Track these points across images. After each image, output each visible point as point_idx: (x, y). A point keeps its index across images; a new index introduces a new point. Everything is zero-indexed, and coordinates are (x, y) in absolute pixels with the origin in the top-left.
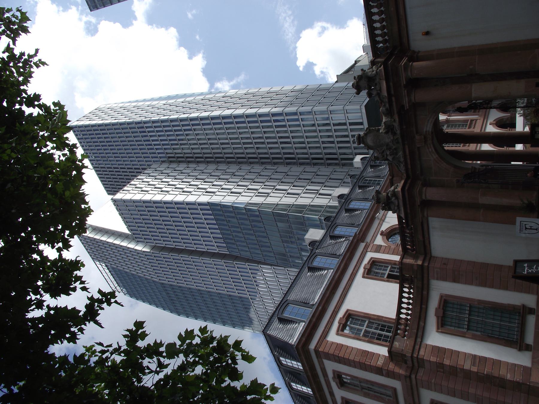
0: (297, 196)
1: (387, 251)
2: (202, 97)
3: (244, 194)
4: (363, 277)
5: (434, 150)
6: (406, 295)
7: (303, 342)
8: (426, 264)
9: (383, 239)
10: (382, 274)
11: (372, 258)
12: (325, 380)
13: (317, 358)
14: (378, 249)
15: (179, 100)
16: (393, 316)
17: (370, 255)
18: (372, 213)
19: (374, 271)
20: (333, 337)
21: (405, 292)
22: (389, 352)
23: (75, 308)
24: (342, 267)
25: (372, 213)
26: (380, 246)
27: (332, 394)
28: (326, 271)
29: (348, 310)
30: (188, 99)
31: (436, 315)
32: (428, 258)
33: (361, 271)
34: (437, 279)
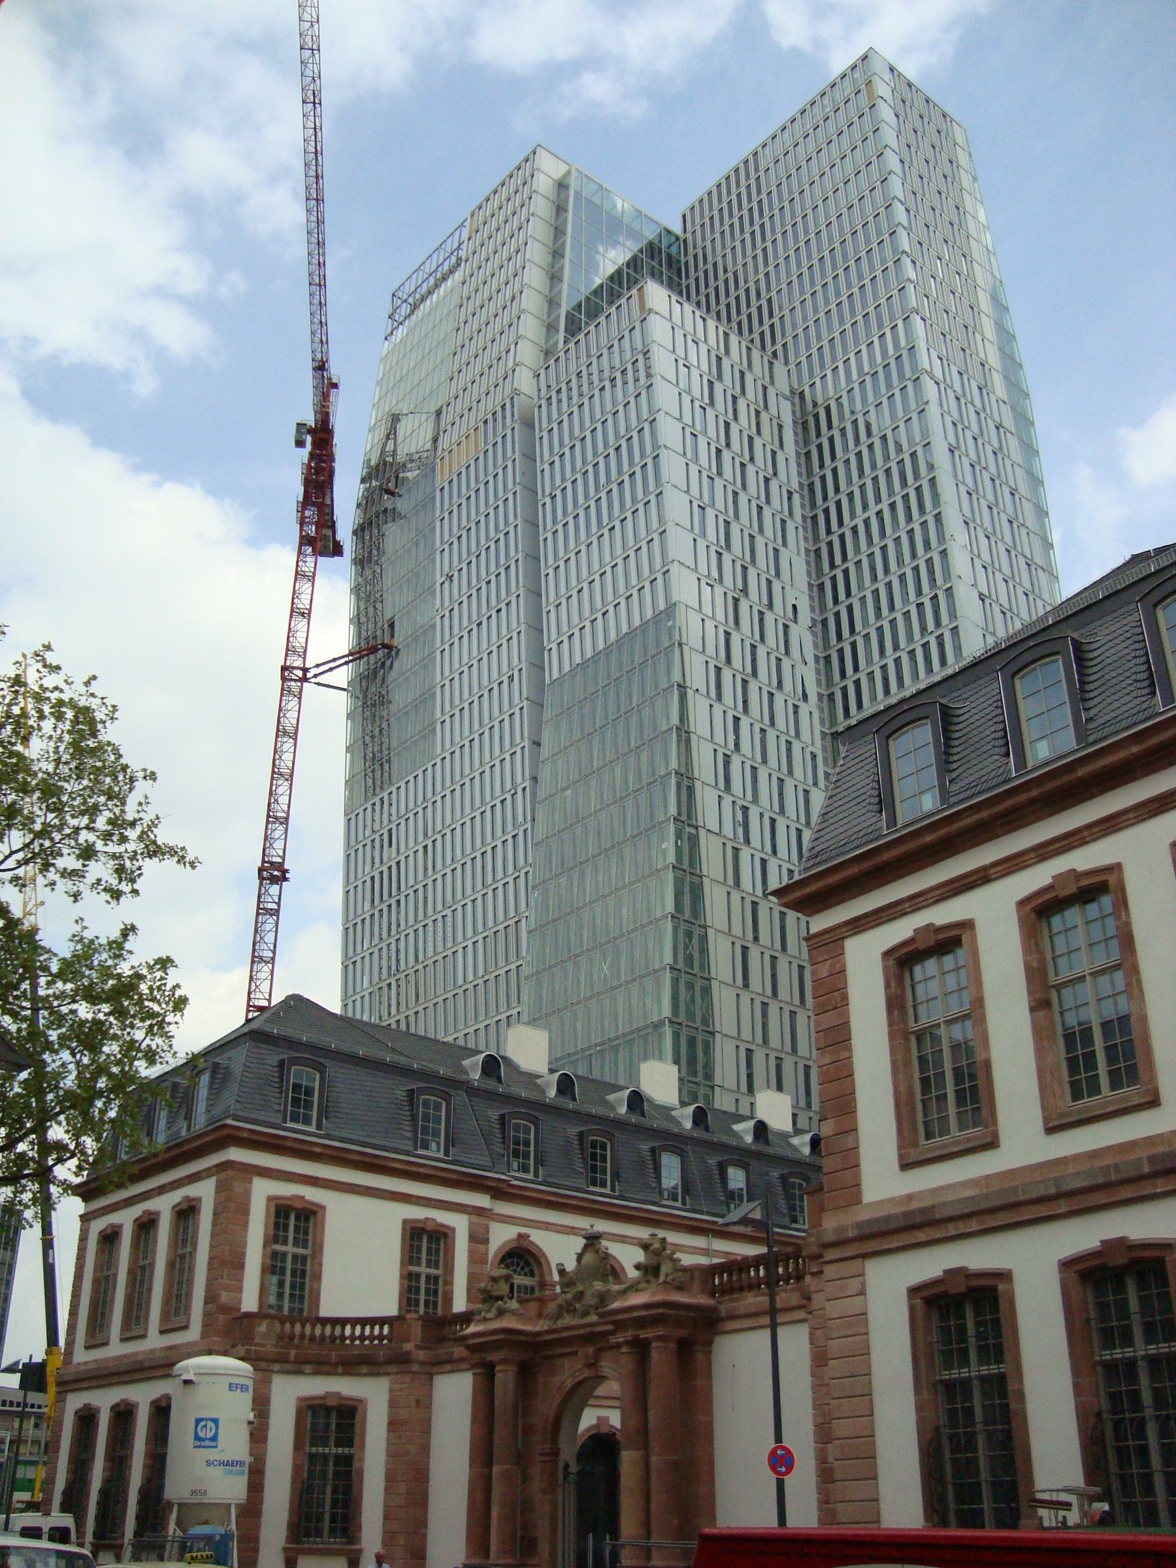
0: (731, 881)
1: (476, 1259)
2: (1023, 488)
3: (718, 709)
4: (405, 1222)
5: (577, 1379)
6: (358, 1331)
7: (239, 1134)
8: (416, 1368)
9: (512, 1240)
10: (419, 1259)
11: (453, 1230)
12: (181, 1179)
13: (217, 1166)
14: (478, 1238)
15: (1006, 411)
16: (323, 1313)
17: (460, 1224)
18: (1058, 845)
19: (424, 1242)
20: (262, 1191)
21: (372, 1329)
22: (249, 1315)
23: (81, 1216)
24: (422, 1170)
25: (574, 1202)
26: (486, 1241)
27: (161, 1190)
28: (409, 1135)
29: (323, 1208)
30: (1013, 443)
31: (328, 1395)
32: (428, 1368)
33: (418, 1213)
34: (391, 1391)
